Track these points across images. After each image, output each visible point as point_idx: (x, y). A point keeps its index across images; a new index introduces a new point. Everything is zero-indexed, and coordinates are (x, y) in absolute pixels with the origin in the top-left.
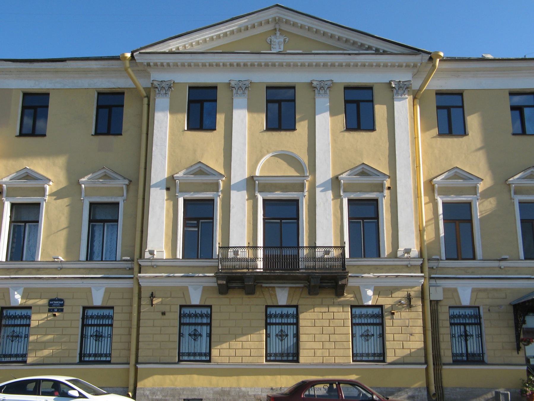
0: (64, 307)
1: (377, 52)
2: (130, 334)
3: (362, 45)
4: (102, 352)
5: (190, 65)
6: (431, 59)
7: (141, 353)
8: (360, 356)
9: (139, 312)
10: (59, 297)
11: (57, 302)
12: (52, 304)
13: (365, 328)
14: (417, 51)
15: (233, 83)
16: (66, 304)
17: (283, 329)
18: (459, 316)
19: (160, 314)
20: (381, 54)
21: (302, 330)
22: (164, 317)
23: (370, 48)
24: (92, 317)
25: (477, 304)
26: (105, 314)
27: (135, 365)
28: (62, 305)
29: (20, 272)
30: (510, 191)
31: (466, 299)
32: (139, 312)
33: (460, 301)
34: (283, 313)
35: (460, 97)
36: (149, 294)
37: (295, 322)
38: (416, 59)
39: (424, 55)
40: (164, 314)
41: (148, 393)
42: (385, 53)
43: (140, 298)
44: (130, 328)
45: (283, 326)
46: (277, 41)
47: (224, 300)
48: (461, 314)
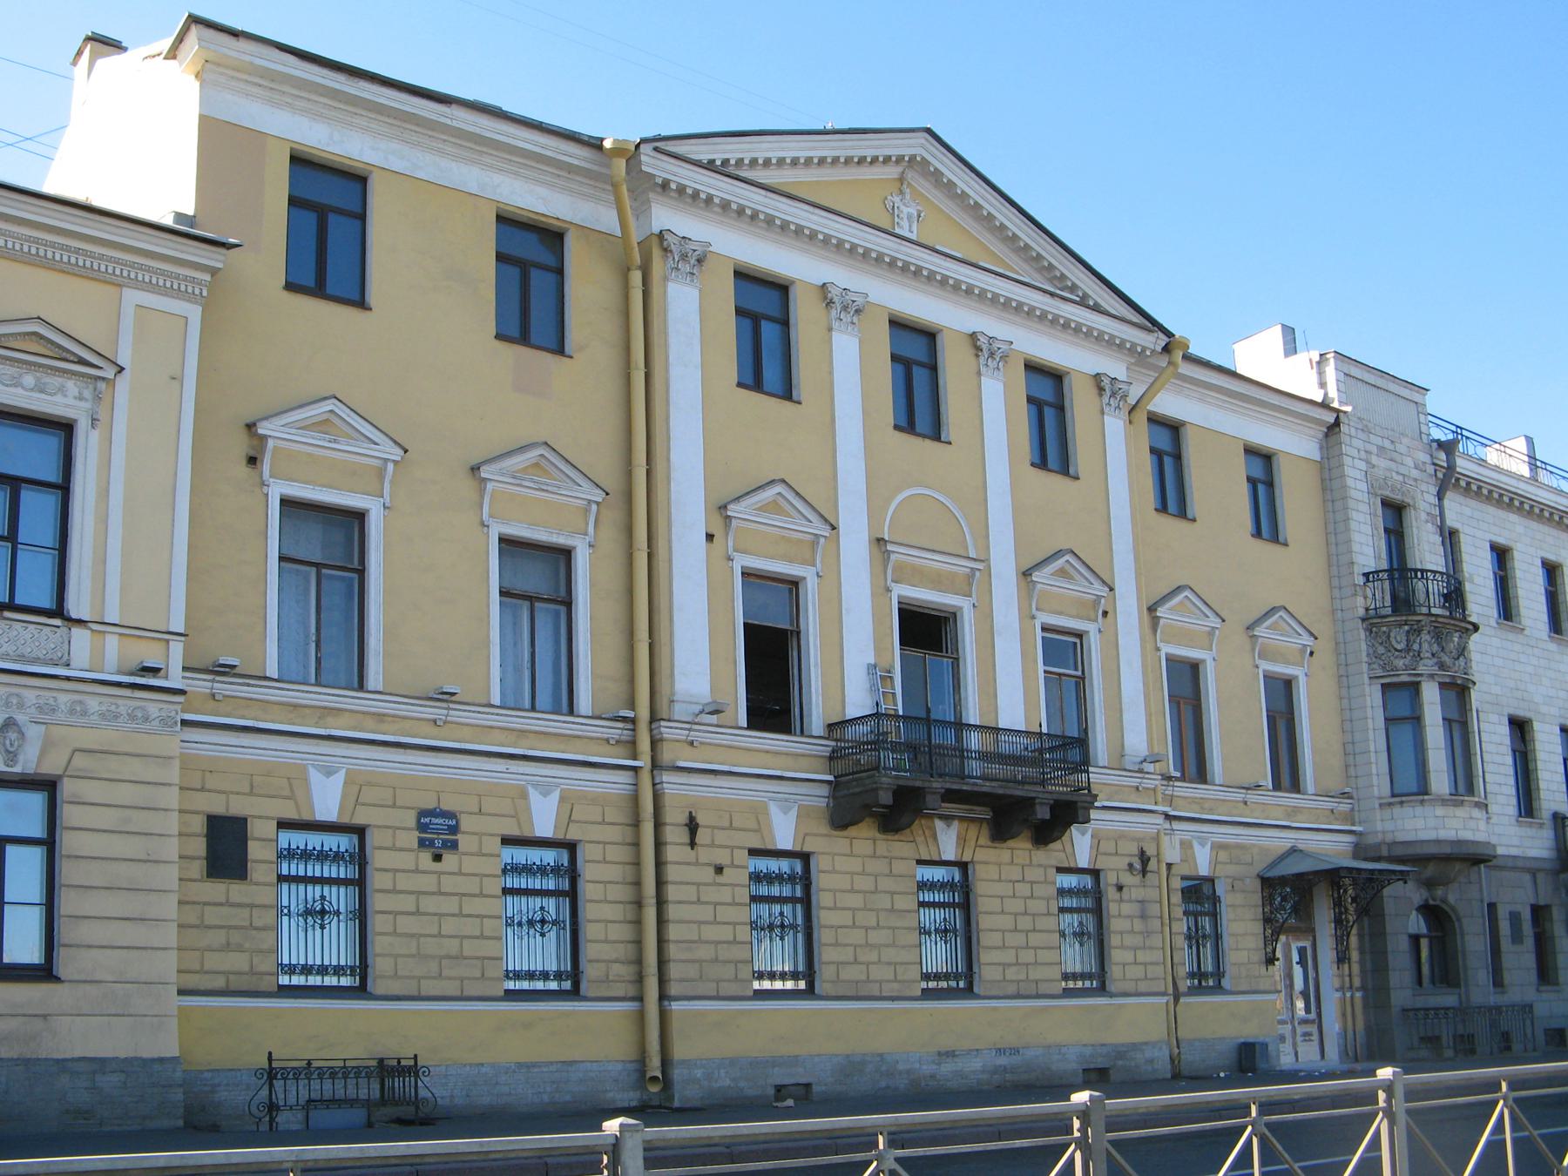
0: (459, 837)
1: (1083, 302)
2: (638, 922)
3: (1063, 277)
4: (326, 963)
5: (754, 216)
6: (1166, 349)
7: (674, 971)
8: (301, 973)
9: (659, 864)
10: (445, 807)
11: (440, 821)
12: (426, 825)
13: (315, 891)
14: (1154, 325)
15: (834, 293)
16: (464, 826)
17: (326, 893)
18: (306, 855)
19: (711, 870)
20: (1088, 307)
21: (377, 902)
22: (720, 879)
23: (1073, 288)
24: (337, 857)
25: (359, 819)
26: (310, 847)
27: (661, 1005)
28: (454, 830)
29: (330, 720)
30: (1253, 650)
31: (327, 801)
32: (659, 864)
33: (773, 838)
34: (326, 848)
35: (358, 186)
36: (683, 818)
37: (799, 894)
38: (1154, 341)
39: (1161, 336)
40: (719, 870)
41: (699, 1073)
42: (1097, 309)
43: (658, 825)
44: (639, 904)
45: (326, 888)
46: (905, 210)
47: (840, 842)
48: (326, 848)
